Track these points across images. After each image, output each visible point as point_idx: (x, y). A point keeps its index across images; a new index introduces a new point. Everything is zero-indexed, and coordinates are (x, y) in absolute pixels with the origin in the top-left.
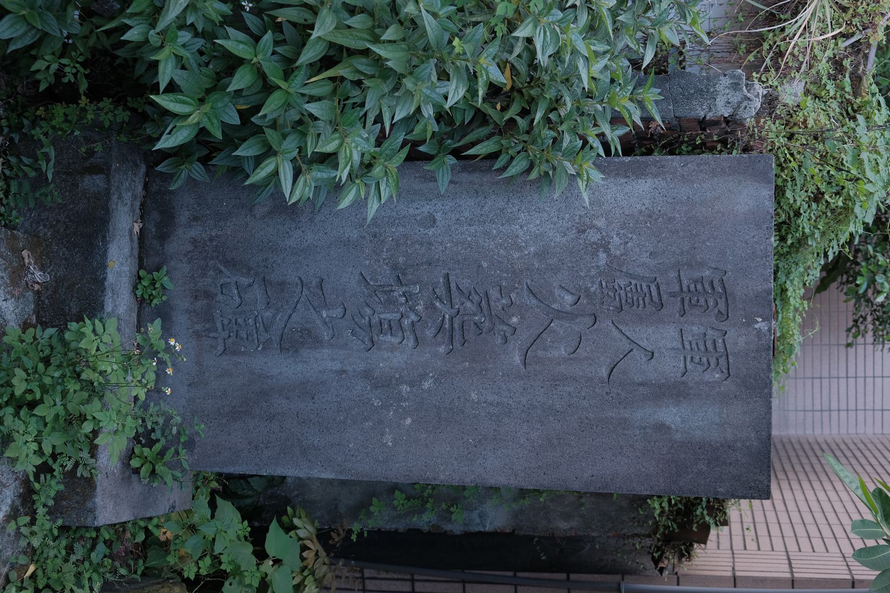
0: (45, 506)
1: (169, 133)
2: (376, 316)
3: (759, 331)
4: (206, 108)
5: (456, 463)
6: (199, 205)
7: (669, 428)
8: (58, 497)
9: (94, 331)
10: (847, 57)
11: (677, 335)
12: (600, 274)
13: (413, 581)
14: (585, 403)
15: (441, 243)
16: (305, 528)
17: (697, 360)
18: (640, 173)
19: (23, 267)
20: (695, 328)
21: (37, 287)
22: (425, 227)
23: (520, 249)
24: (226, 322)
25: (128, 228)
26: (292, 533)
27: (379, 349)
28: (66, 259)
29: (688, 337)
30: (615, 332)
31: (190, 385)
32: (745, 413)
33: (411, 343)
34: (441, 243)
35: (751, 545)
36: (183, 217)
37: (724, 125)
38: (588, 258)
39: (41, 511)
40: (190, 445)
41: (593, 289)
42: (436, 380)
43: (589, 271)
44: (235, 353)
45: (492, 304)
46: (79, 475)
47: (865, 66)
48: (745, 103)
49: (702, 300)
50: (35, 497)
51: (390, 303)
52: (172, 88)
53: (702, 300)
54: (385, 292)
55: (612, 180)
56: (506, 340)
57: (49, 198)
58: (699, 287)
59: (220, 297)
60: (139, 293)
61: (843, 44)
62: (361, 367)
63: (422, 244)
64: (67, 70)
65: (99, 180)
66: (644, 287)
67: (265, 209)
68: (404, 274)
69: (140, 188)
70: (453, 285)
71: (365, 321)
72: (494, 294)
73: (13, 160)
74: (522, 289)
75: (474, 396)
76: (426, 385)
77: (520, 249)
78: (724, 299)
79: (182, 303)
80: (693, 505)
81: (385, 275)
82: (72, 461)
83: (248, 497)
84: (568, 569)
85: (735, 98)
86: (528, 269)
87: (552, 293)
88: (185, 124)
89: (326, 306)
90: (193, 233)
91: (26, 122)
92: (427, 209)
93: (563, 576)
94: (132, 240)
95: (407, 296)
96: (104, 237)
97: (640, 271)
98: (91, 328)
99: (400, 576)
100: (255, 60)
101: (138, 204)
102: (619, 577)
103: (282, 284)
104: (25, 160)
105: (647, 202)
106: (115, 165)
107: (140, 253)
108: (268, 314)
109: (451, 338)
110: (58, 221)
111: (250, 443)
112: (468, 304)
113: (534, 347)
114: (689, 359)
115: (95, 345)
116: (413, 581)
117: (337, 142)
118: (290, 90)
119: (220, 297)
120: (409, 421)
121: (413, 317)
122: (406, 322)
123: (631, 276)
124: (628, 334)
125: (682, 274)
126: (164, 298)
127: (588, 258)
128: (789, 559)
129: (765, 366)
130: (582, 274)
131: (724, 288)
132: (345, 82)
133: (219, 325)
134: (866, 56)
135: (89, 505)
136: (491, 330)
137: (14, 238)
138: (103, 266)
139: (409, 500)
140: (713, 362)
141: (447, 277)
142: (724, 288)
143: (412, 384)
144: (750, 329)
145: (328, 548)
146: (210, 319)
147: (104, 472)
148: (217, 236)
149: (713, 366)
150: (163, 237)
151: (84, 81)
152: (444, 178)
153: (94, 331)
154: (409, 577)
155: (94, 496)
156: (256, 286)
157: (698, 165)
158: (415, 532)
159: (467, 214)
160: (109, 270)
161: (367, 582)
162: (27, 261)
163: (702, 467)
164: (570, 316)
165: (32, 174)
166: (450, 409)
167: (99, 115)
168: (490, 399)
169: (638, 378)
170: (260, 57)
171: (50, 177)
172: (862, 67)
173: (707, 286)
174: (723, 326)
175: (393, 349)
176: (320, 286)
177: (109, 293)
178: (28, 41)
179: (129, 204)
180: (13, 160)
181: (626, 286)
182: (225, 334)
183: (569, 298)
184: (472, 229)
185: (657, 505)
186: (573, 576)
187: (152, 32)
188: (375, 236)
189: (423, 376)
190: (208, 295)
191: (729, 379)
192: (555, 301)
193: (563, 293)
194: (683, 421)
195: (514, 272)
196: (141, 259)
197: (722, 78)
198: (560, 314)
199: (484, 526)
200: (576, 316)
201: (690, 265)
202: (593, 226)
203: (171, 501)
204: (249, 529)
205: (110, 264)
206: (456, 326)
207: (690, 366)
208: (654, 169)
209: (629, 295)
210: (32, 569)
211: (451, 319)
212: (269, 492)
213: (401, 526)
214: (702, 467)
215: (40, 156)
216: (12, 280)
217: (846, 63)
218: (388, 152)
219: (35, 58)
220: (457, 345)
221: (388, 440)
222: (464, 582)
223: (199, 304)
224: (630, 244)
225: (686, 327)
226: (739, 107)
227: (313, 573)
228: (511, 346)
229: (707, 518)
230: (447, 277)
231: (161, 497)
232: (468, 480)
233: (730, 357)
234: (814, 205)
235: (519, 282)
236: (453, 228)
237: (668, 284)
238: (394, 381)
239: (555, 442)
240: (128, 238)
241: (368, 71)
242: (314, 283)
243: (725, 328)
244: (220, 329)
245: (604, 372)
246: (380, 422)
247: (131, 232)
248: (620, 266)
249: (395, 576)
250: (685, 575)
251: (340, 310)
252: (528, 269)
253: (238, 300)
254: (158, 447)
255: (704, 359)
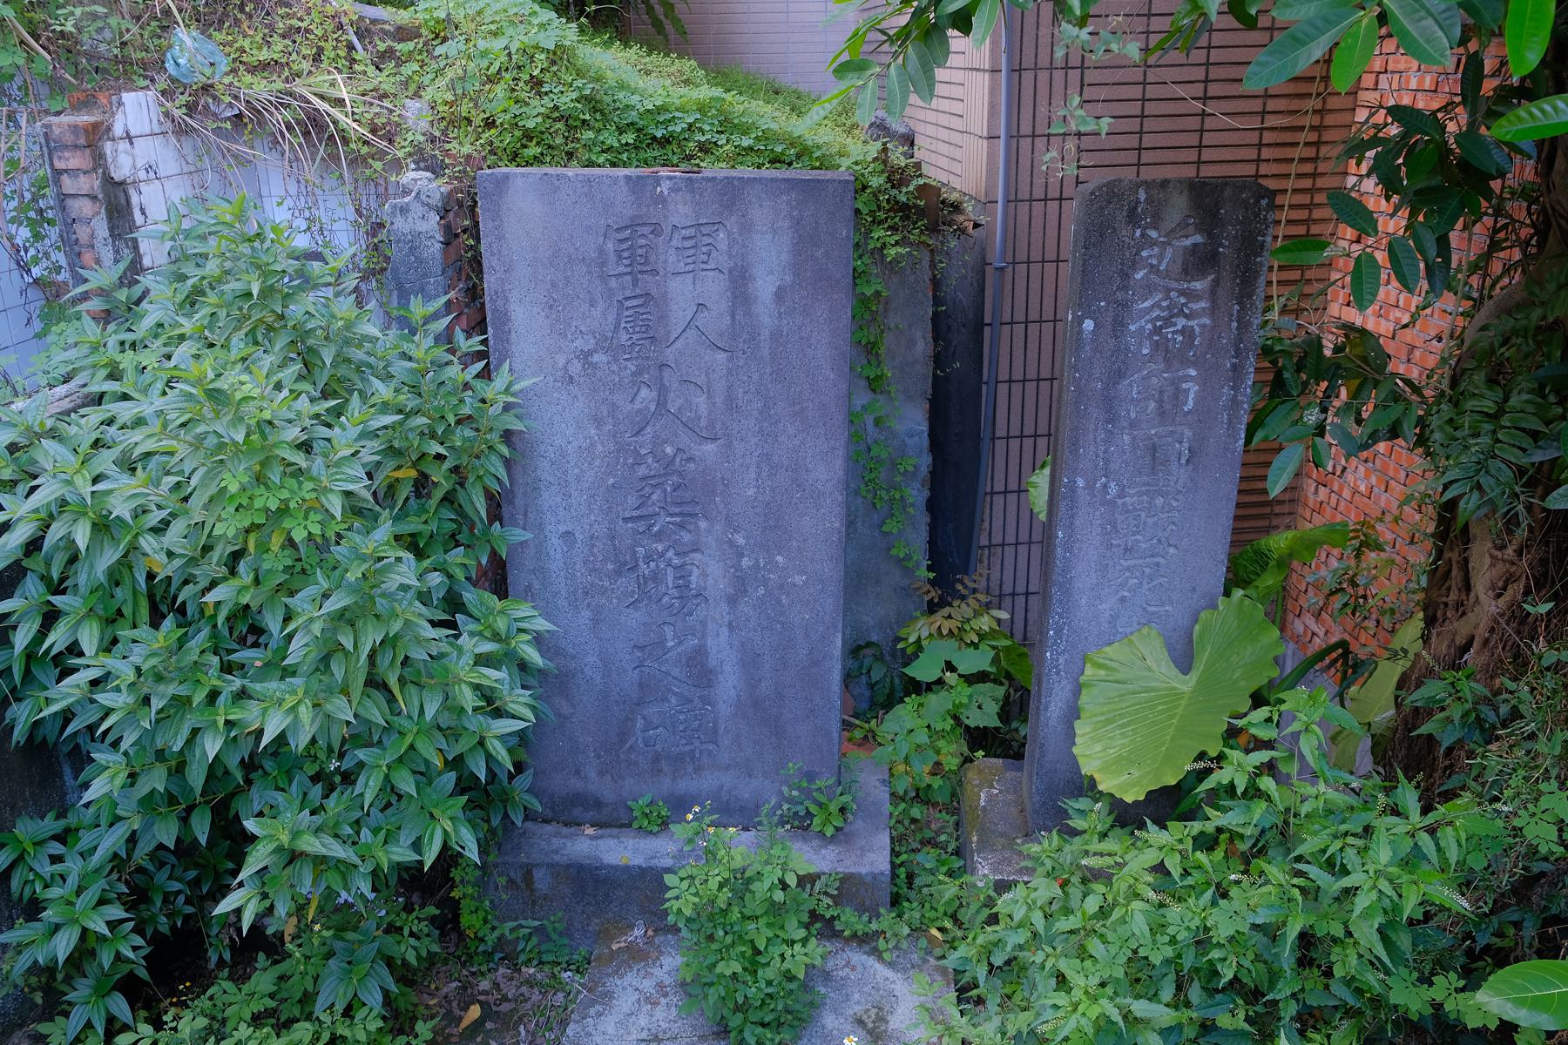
0: (870, 922)
1: (463, 848)
2: (670, 592)
3: (671, 190)
4: (436, 813)
5: (823, 511)
6: (563, 769)
7: (779, 288)
8: (861, 909)
9: (677, 898)
10: (376, 45)
11: (679, 278)
12: (616, 360)
13: (992, 493)
14: (755, 377)
15: (591, 526)
16: (920, 629)
17: (705, 258)
18: (504, 318)
19: (629, 948)
20: (671, 259)
21: (650, 933)
22: (575, 541)
23: (593, 445)
24: (684, 741)
25: (589, 842)
26: (924, 643)
27: (705, 589)
28: (621, 904)
29: (681, 267)
30: (679, 344)
31: (750, 776)
32: (761, 206)
33: (697, 556)
34: (591, 526)
35: (957, 108)
36: (576, 784)
37: (451, 215)
38: (599, 373)
39: (874, 926)
40: (811, 776)
41: (633, 368)
42: (735, 531)
43: (613, 372)
44: (715, 731)
45: (652, 473)
46: (836, 893)
47: (385, 22)
48: (423, 197)
49: (640, 251)
50: (860, 933)
51: (656, 577)
52: (417, 846)
53: (640, 251)
54: (646, 582)
55: (513, 347)
56: (690, 459)
57: (557, 925)
58: (625, 254)
59: (658, 747)
60: (656, 829)
61: (360, 54)
62: (725, 607)
63: (593, 546)
64: (415, 929)
65: (538, 874)
66: (627, 313)
67: (564, 703)
68: (625, 563)
69: (548, 828)
70: (635, 513)
71: (677, 603)
72: (642, 471)
73: (522, 958)
74: (636, 442)
75: (751, 492)
76: (741, 541)
77: (593, 445)
78: (638, 228)
79: (666, 784)
80: (897, 202)
81: (626, 583)
82: (822, 897)
83: (892, 683)
84: (979, 325)
85: (418, 210)
86: (614, 436)
87: (639, 411)
88: (453, 834)
89: (662, 642)
90: (593, 775)
91: (481, 948)
92: (555, 541)
93: (987, 330)
94: (602, 837)
95: (648, 559)
96: (597, 868)
97: (611, 318)
98: (673, 902)
99: (988, 507)
100: (384, 768)
101: (565, 830)
102: (988, 268)
103: (641, 685)
104: (520, 947)
105: (535, 310)
106: (523, 858)
107: (616, 827)
108: (673, 700)
109: (690, 515)
110: (583, 912)
111: (808, 717)
112: (654, 497)
113: (697, 430)
114: (705, 266)
115: (690, 898)
116: (992, 493)
117: (464, 686)
118: (415, 729)
119: (658, 747)
120: (779, 559)
121: (670, 554)
122: (676, 561)
123: (617, 327)
124: (679, 331)
125: (612, 273)
126: (661, 803)
127: (599, 373)
128: (971, 69)
129: (710, 184)
130: (617, 379)
131: (626, 228)
132: (406, 674)
133: (687, 748)
134: (374, 21)
135: (869, 879)
136: (680, 474)
137: (599, 958)
138: (627, 868)
139: (893, 515)
140: (706, 240)
141: (626, 520)
142: (626, 228)
143: (741, 555)
144: (669, 199)
145: (943, 603)
146: (681, 757)
147: (836, 865)
148: (594, 751)
149: (711, 240)
150: (598, 804)
151: (427, 909)
152: (517, 535)
153: (677, 898)
154: (988, 498)
155: (860, 874)
156: (645, 712)
157: (493, 254)
158: (931, 506)
159: (559, 500)
160: (631, 863)
161: (993, 542)
162: (623, 945)
163: (820, 253)
164: (663, 391)
165: (534, 940)
166: (765, 515)
167: (468, 882)
168: (754, 476)
169: (727, 320)
170: (381, 763)
171: (537, 923)
172: (387, 27)
173: (624, 246)
174: (667, 230)
175: (704, 575)
176: (642, 648)
177: (655, 862)
178: (385, 972)
179: (563, 840)
180: (522, 958)
181: (628, 333)
182: (697, 743)
183: (644, 392)
184: (575, 494)
185: (893, 251)
186: (987, 321)
187: (361, 870)
188: (587, 593)
189: (731, 543)
190: (656, 759)
191: (725, 222)
192: (647, 408)
193: (639, 399)
194: (772, 272)
195: (618, 451)
196: (622, 826)
197: (395, 227)
198: (661, 402)
199: (923, 431)
200: (663, 385)
201: (603, 264)
202: (565, 368)
203: (878, 784)
204: (913, 696)
205: (624, 862)
206: (677, 510)
207: (712, 266)
208: (500, 303)
209: (638, 329)
210: (934, 932)
211: (671, 515)
212: (888, 658)
213: (924, 519)
214: (820, 253)
215: (514, 936)
216: (642, 960)
217: (382, 47)
218: (484, 610)
219: (405, 963)
220: (697, 509)
221: (799, 579)
222: (993, 439)
223: (666, 768)
224: (583, 329)
225: (670, 269)
226: (428, 205)
227: (968, 620)
228: (697, 453)
229: (911, 188)
230: (626, 520)
231: (743, 953)
232: (840, 498)
233: (701, 221)
234: (546, 88)
235: (629, 445)
236: (575, 514)
237: (624, 288)
238: (738, 574)
239: (797, 408)
240: (600, 842)
241: (389, 656)
242: (639, 654)
243: (670, 228)
244: (692, 747)
245: (721, 356)
246: (781, 587)
247: (593, 838)
248: (606, 339)
249: (987, 512)
250: (987, 195)
251: (666, 628)
252: (614, 436)
253: (661, 729)
254: (813, 809)
255: (704, 249)
